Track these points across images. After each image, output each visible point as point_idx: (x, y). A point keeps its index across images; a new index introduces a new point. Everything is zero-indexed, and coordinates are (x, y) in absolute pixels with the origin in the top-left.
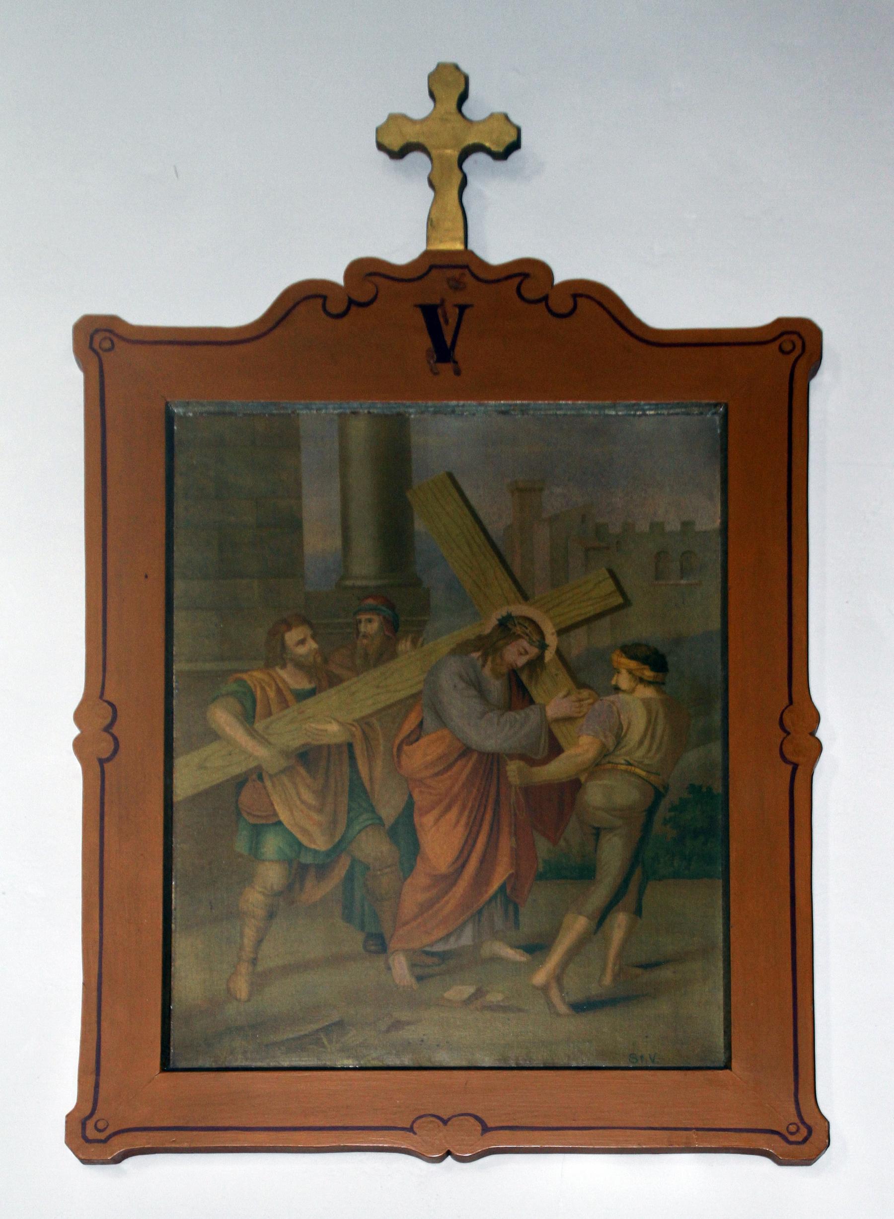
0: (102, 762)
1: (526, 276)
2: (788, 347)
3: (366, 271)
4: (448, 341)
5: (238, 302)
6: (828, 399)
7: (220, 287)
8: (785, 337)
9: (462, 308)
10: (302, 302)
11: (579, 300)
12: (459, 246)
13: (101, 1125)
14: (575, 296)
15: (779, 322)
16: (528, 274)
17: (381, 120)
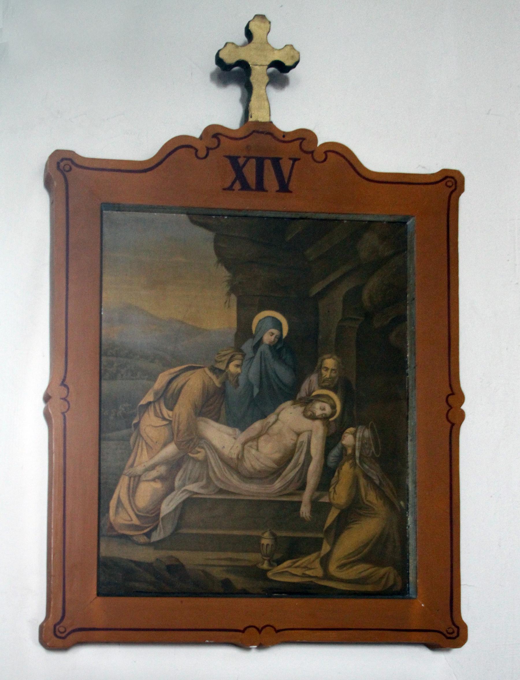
0: (63, 413)
1: (303, 139)
2: (67, 168)
3: (215, 134)
4: (286, 174)
5: (142, 147)
6: (467, 205)
7: (129, 136)
8: (448, 179)
9: (230, 188)
10: (178, 148)
11: (329, 154)
12: (266, 120)
13: (62, 630)
14: (326, 153)
15: (444, 171)
16: (304, 137)
17: (42, 405)
